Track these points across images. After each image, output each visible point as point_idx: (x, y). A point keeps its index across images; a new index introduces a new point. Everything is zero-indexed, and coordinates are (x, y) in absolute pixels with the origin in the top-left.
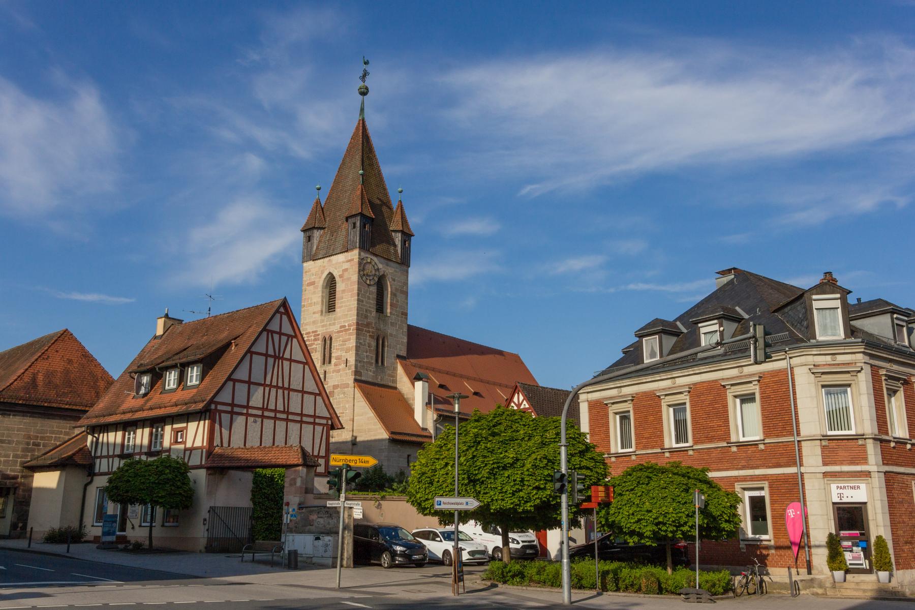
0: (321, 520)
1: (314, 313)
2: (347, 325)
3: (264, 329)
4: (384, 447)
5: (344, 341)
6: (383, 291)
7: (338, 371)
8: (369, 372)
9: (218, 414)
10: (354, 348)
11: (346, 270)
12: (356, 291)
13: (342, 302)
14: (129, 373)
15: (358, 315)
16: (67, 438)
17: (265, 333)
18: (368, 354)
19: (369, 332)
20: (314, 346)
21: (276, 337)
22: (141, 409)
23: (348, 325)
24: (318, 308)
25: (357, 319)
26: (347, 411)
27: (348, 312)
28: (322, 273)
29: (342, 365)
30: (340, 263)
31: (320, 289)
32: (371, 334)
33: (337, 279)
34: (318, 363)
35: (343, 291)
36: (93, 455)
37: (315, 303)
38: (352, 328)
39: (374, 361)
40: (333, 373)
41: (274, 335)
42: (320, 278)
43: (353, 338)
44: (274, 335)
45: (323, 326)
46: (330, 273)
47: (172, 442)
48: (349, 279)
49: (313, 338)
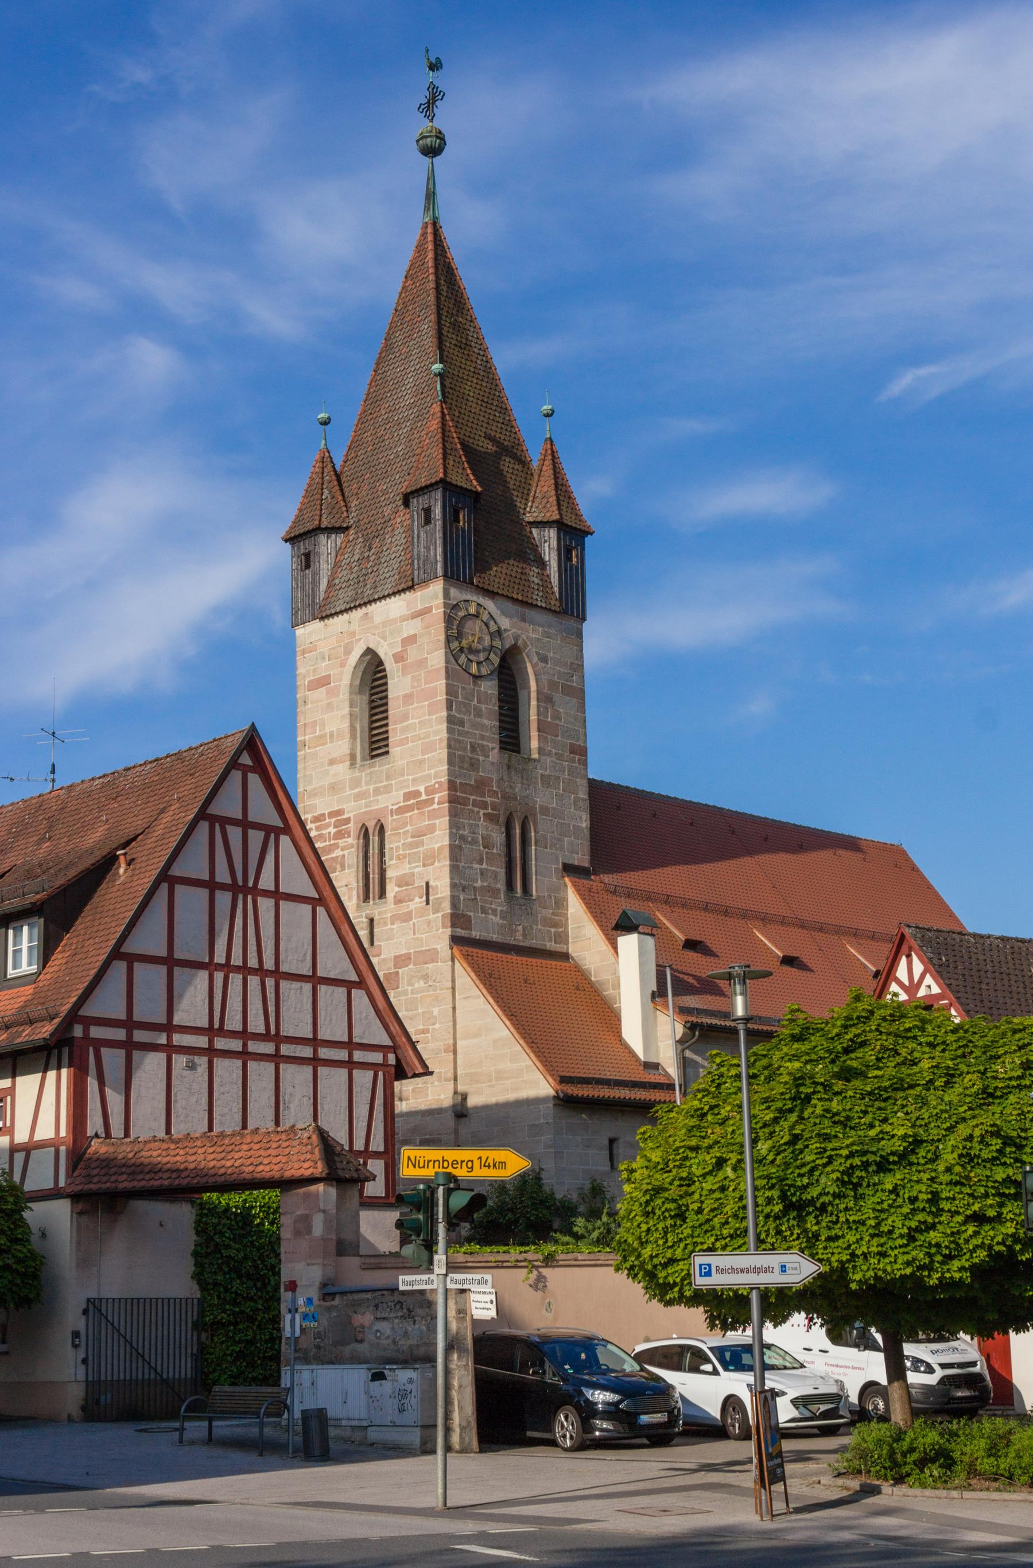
0: (385, 1327)
1: (332, 762)
5: (419, 834)
6: (515, 690)
7: (407, 917)
8: (491, 917)
9: (91, 1049)
10: (446, 852)
11: (411, 640)
12: (442, 697)
13: (404, 730)
15: (450, 762)
17: (204, 826)
18: (484, 866)
19: (484, 805)
20: (338, 853)
21: (235, 834)
24: (342, 747)
25: (450, 773)
26: (437, 1026)
28: (348, 652)
29: (417, 900)
30: (394, 621)
32: (490, 810)
33: (389, 665)
34: (350, 898)
35: (408, 698)
37: (332, 734)
38: (437, 796)
39: (501, 885)
40: (392, 923)
42: (342, 665)
43: (443, 823)
45: (358, 797)
46: (369, 651)
48: (421, 663)
49: (332, 830)
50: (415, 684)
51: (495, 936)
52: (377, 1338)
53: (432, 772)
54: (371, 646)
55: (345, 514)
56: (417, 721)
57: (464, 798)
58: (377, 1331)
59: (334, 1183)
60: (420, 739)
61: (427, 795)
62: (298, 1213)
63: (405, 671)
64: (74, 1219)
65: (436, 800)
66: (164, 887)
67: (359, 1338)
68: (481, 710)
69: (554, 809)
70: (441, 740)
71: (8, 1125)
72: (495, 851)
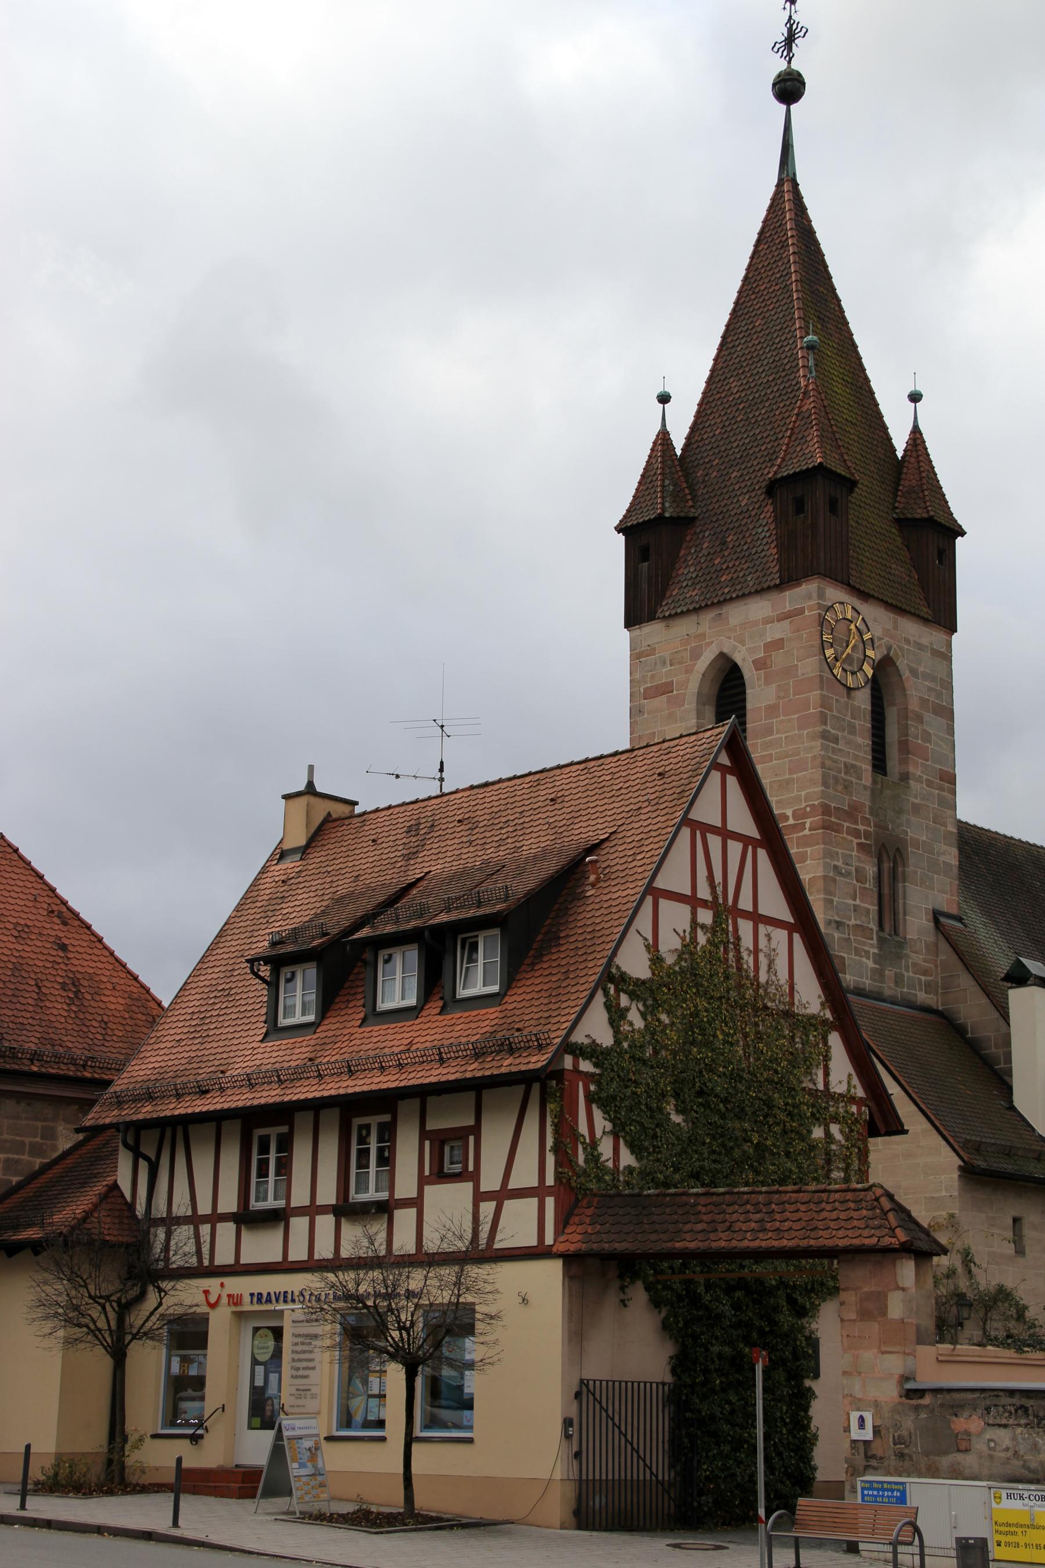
0: (1003, 1437)
2: (789, 812)
3: (686, 821)
4: (944, 1193)
8: (864, 960)
11: (778, 644)
14: (247, 961)
16: (38, 1162)
17: (686, 832)
18: (858, 902)
19: (857, 834)
21: (715, 842)
22: (298, 1075)
23: (794, 813)
27: (791, 773)
28: (696, 655)
31: (690, 705)
32: (863, 840)
33: (748, 673)
36: (140, 1209)
38: (808, 822)
39: (873, 926)
41: (710, 837)
42: (688, 671)
44: (710, 837)
46: (722, 656)
47: (427, 1173)
48: (789, 671)
50: (782, 694)
51: (867, 982)
52: (990, 1449)
53: (803, 793)
54: (725, 651)
55: (690, 503)
56: (783, 736)
57: (838, 824)
58: (990, 1440)
59: (913, 1256)
60: (787, 756)
61: (795, 819)
62: (866, 1289)
63: (768, 681)
64: (566, 1284)
65: (807, 826)
66: (649, 899)
67: (962, 1447)
68: (854, 727)
69: (923, 841)
70: (814, 758)
71: (471, 1168)
72: (867, 886)
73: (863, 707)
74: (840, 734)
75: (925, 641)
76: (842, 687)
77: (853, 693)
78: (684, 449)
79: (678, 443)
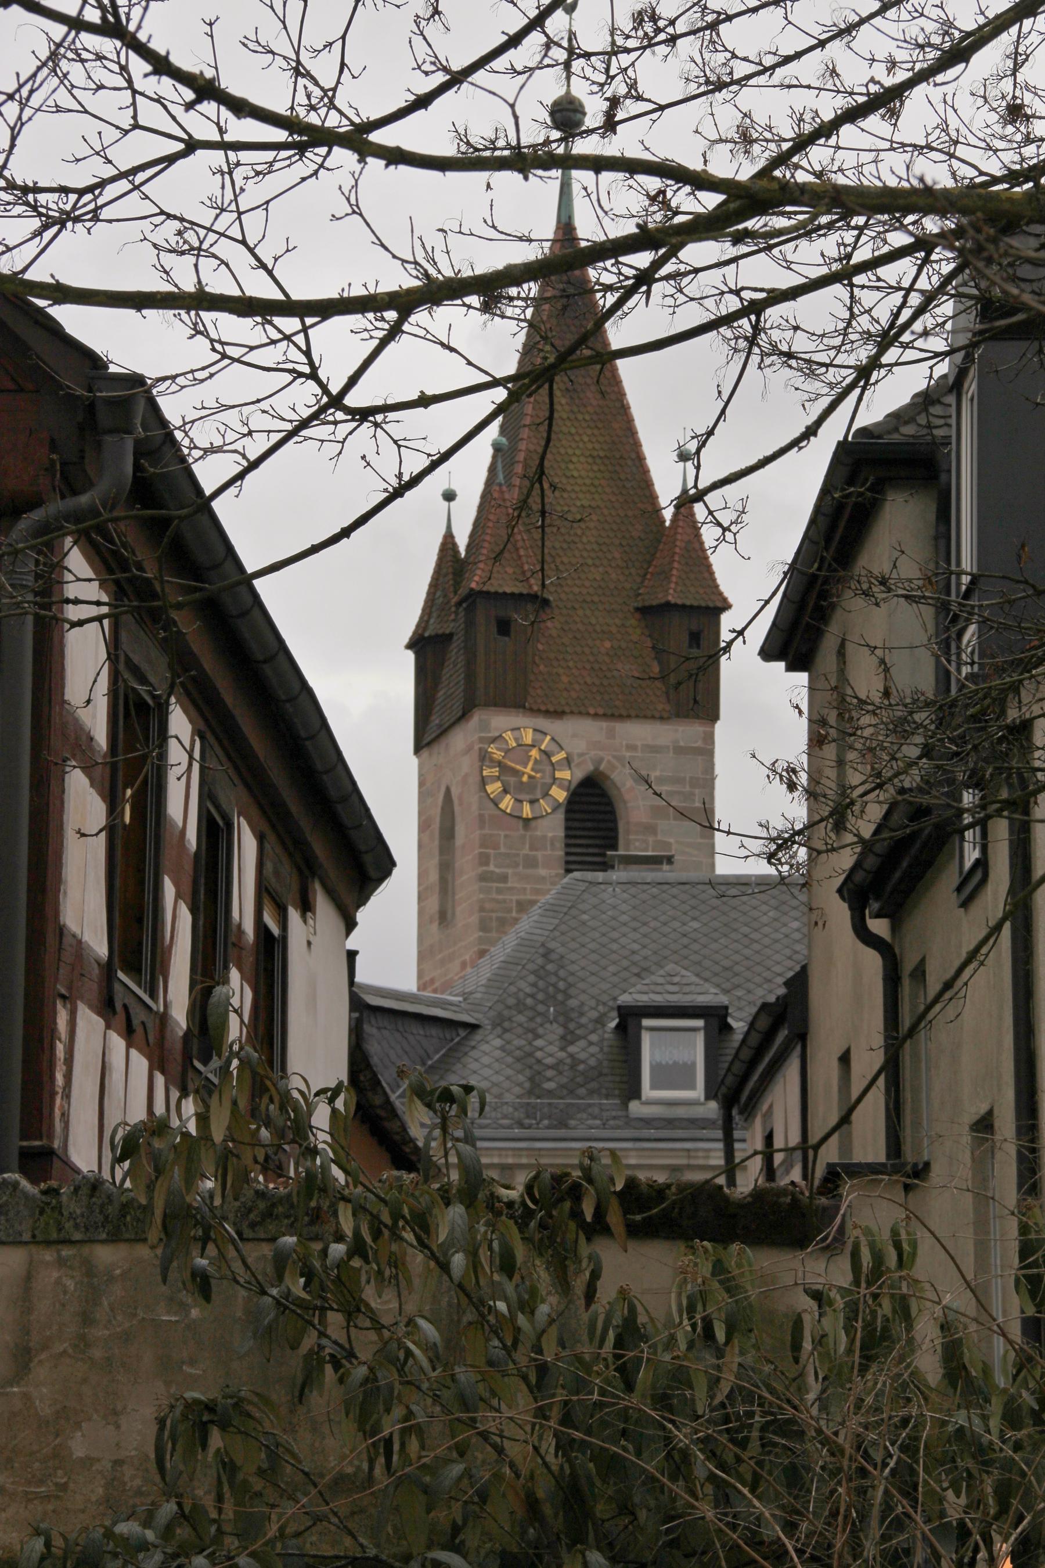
73: (550, 835)
74: (510, 871)
75: (662, 741)
76: (515, 820)
77: (533, 824)
78: (469, 547)
79: (462, 541)
